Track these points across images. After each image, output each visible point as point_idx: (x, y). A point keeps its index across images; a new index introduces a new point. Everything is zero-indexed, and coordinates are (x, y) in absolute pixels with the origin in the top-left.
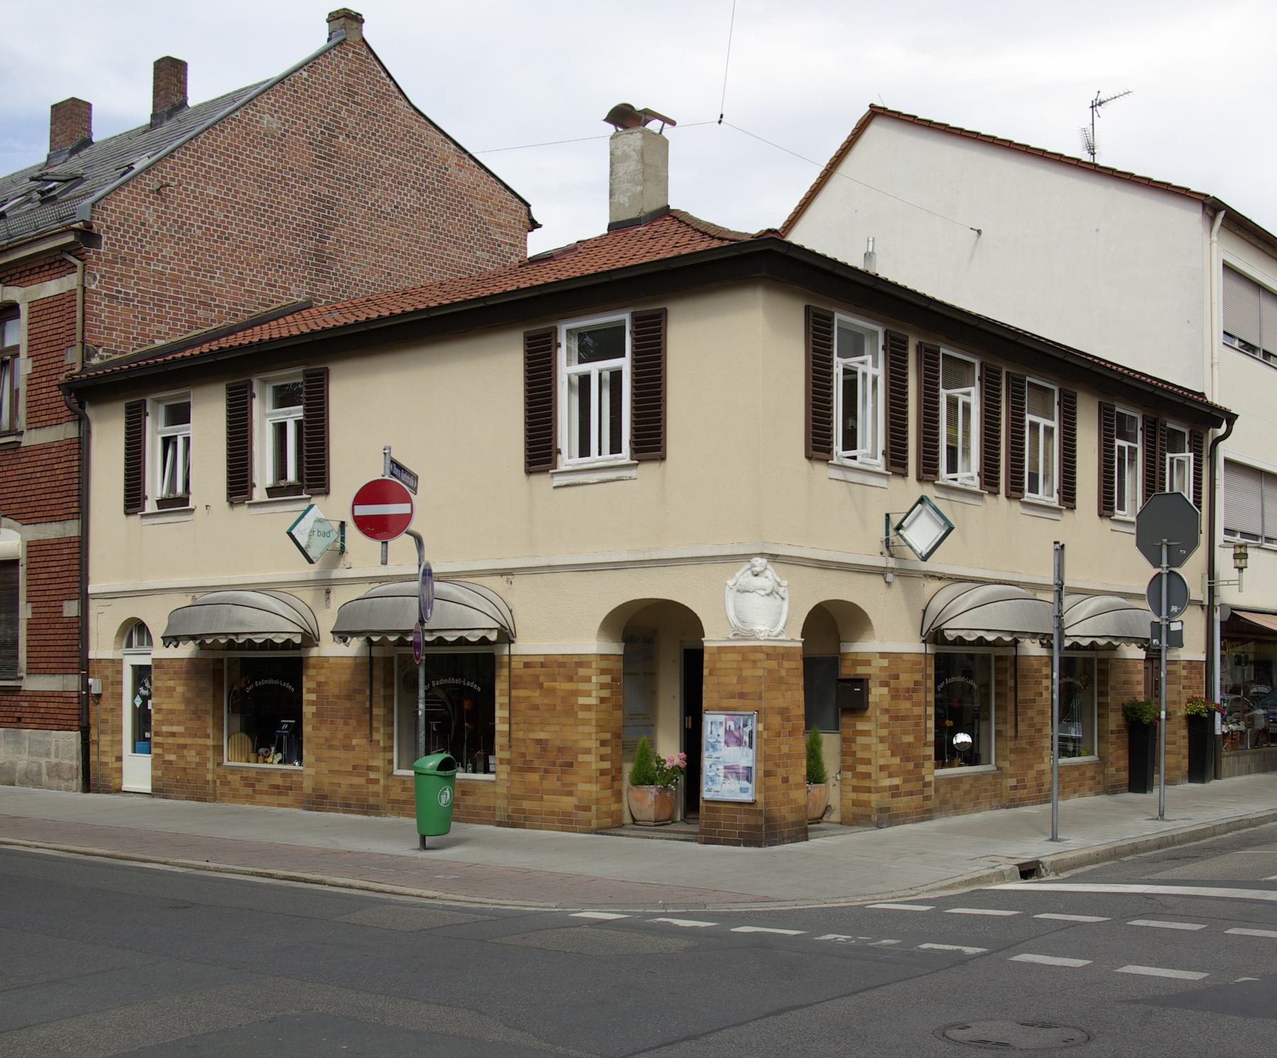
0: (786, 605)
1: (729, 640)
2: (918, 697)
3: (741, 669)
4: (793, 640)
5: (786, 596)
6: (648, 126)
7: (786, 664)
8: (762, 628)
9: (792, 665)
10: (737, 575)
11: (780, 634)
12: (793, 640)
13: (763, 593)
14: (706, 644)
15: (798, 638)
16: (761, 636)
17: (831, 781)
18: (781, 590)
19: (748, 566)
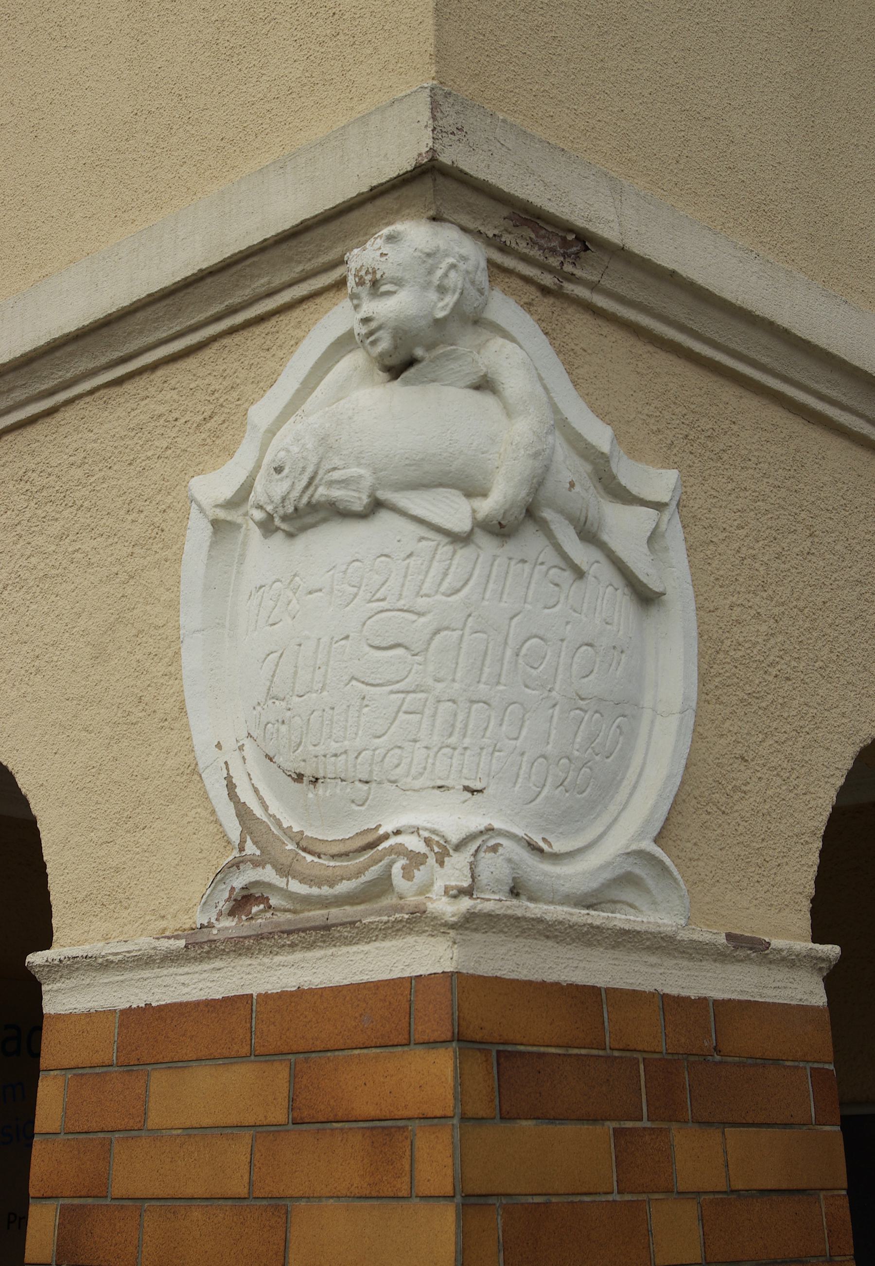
0: (671, 668)
1: (200, 947)
2: (263, 1119)
3: (280, 1207)
4: (747, 947)
5: (673, 575)
6: (606, 448)
7: (698, 1157)
8: (454, 819)
9: (755, 1157)
10: (262, 412)
11: (624, 881)
12: (747, 947)
13: (455, 512)
14: (57, 1000)
15: (792, 932)
16: (438, 890)
17: (811, 945)
18: (626, 528)
19: (338, 318)
